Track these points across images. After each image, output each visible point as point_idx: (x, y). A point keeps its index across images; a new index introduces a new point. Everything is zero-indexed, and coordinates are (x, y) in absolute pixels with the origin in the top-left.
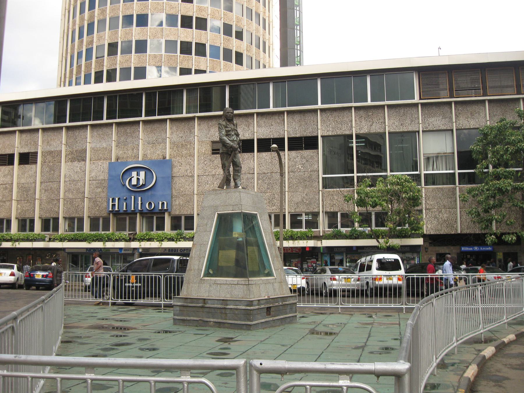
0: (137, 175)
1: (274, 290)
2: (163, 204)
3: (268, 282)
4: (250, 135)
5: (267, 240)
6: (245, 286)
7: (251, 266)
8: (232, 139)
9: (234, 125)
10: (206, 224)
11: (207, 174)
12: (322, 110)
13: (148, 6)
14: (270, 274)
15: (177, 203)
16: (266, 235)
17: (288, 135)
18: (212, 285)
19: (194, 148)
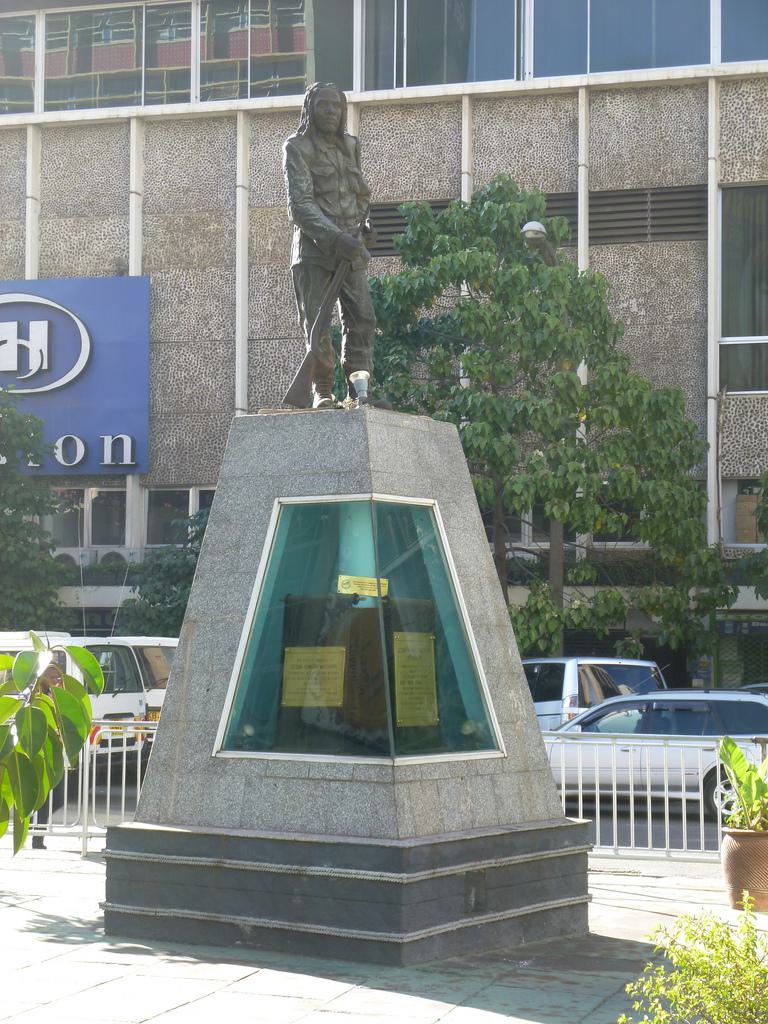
0: (20, 336)
1: (498, 800)
2: (118, 445)
3: (473, 771)
4: (446, 184)
5: (470, 606)
6: (382, 790)
7: (414, 707)
8: (338, 211)
9: (346, 154)
10: (237, 545)
11: (282, 333)
12: (727, 83)
14: (485, 742)
15: (172, 441)
16: (466, 588)
17: (590, 181)
18: (256, 781)
19: (233, 233)
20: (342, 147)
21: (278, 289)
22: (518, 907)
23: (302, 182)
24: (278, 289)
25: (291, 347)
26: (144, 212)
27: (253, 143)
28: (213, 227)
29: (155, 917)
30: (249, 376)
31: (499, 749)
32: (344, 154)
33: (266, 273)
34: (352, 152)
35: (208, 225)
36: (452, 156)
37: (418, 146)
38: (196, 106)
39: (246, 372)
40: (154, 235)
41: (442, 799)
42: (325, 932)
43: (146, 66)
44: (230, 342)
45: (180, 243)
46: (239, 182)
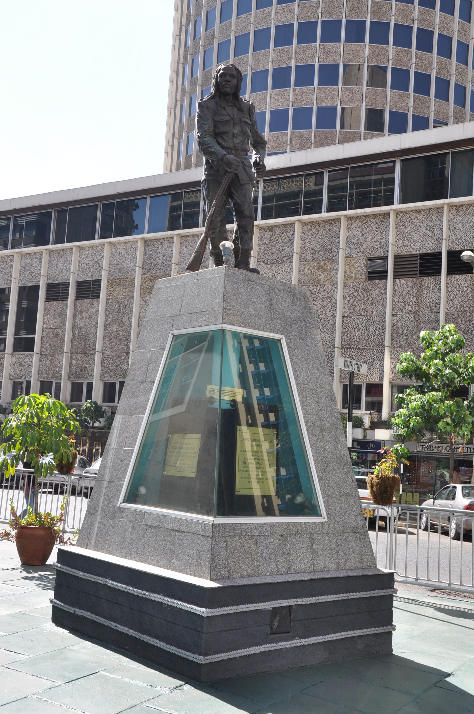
4: (435, 245)
8: (230, 145)
11: (358, 313)
13: (292, 54)
20: (238, 105)
21: (357, 293)
22: (324, 635)
23: (205, 124)
24: (357, 293)
25: (361, 319)
26: (300, 261)
27: (348, 230)
28: (329, 267)
29: (73, 614)
30: (342, 332)
31: (321, 516)
32: (239, 110)
33: (351, 286)
34: (246, 110)
35: (327, 266)
36: (439, 232)
37: (423, 228)
38: (325, 215)
39: (341, 331)
40: (303, 271)
41: (259, 551)
42: (157, 645)
43: (304, 198)
44: (334, 317)
45: (315, 274)
46: (341, 247)
